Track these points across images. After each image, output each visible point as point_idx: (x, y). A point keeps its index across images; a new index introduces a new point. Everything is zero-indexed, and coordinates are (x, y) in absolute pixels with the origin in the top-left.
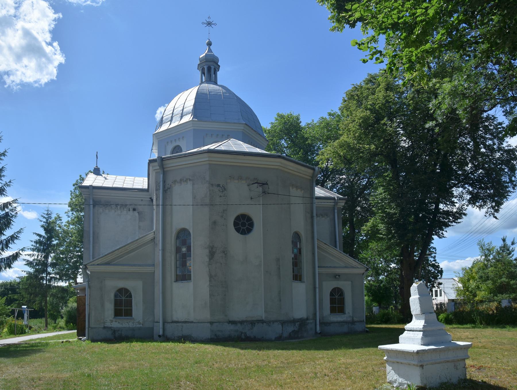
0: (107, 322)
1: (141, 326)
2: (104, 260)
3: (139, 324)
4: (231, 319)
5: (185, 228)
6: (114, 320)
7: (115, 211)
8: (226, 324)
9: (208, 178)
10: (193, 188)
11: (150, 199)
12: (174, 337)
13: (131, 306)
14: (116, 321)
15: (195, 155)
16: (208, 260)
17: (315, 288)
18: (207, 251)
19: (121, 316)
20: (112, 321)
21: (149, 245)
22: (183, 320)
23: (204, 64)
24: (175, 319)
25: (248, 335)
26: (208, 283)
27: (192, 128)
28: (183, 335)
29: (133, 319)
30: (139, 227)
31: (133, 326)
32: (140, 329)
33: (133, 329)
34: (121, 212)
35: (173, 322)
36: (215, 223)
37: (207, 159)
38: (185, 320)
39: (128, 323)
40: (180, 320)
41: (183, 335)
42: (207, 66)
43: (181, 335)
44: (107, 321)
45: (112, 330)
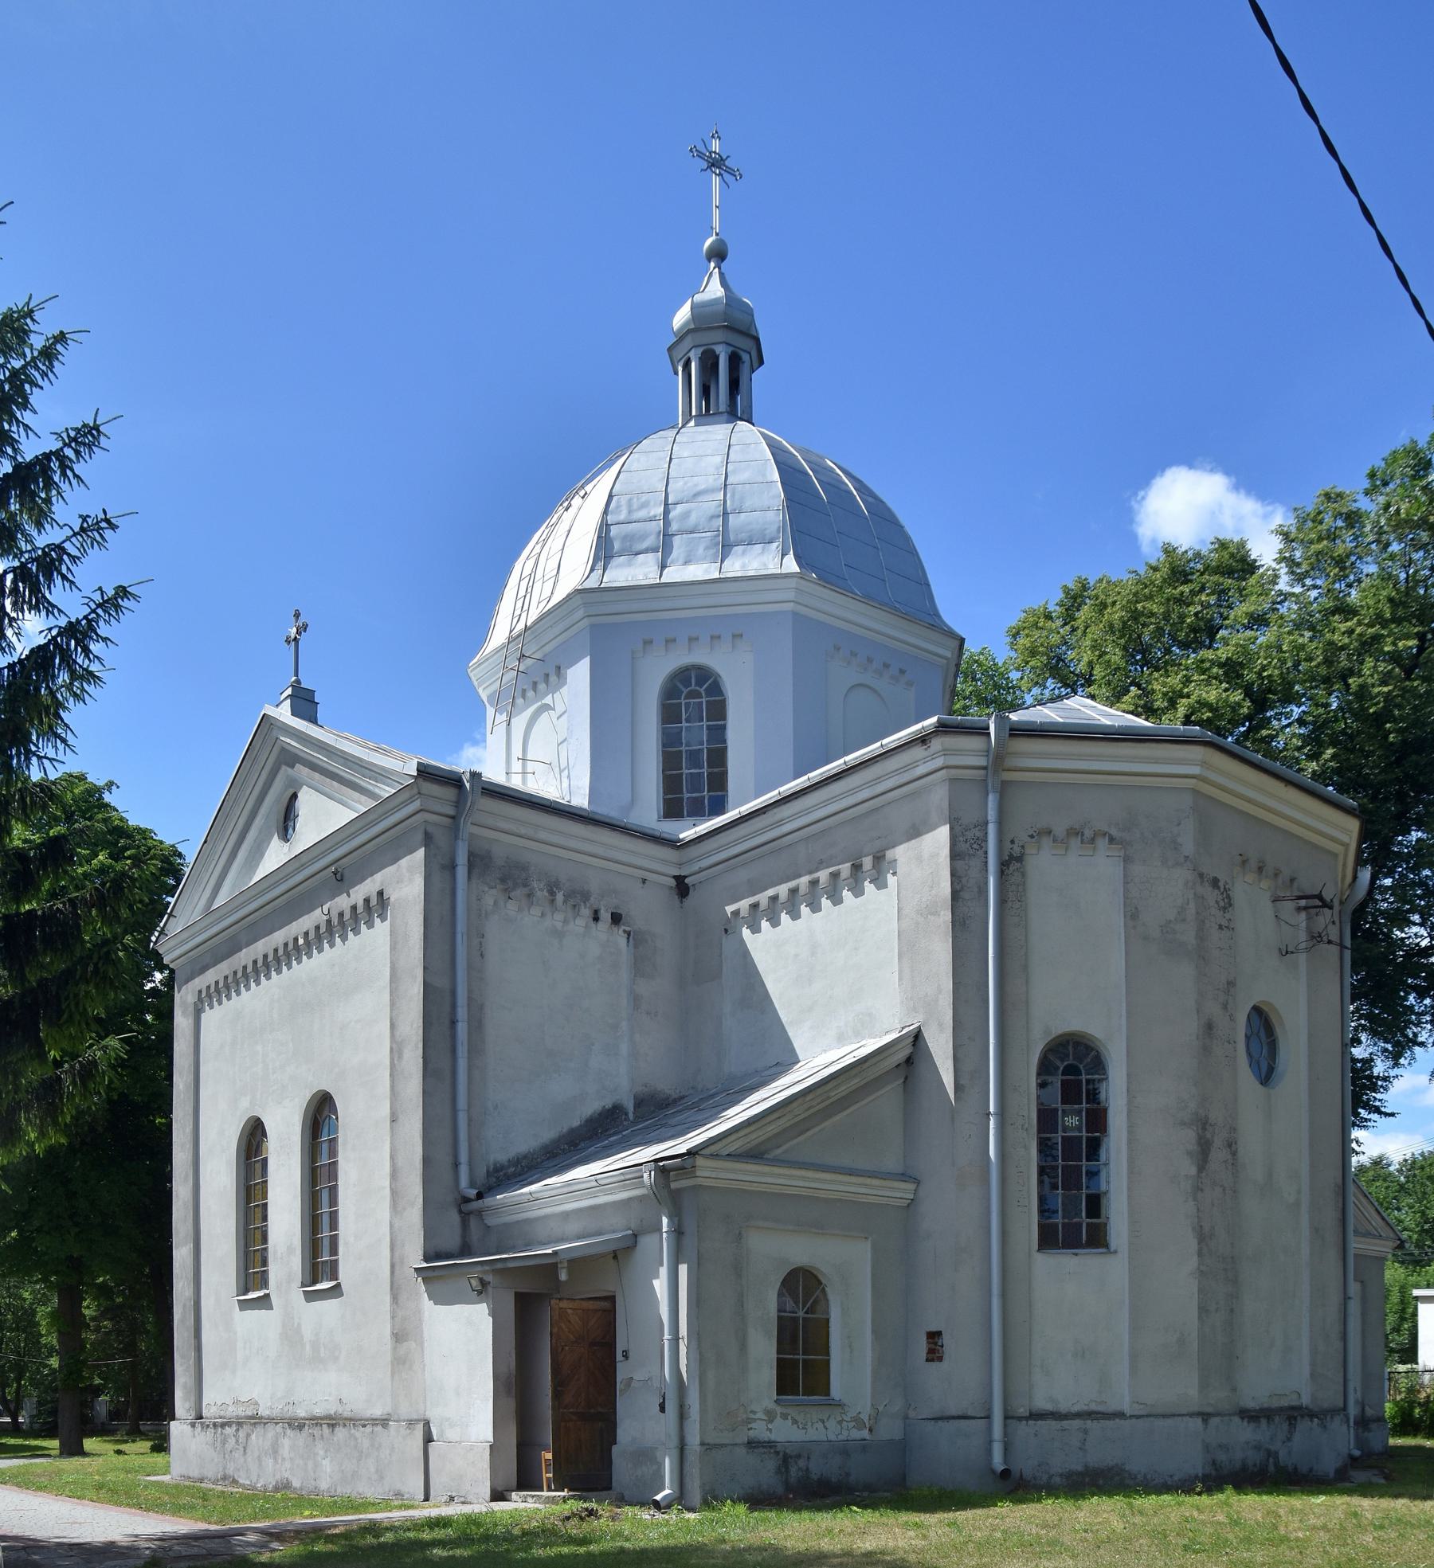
0: (755, 1420)
1: (865, 1434)
2: (753, 1136)
3: (859, 1429)
4: (1251, 1404)
5: (1072, 1034)
6: (779, 1410)
7: (543, 915)
8: (1236, 1419)
9: (1188, 847)
10: (1125, 876)
11: (673, 882)
12: (1051, 1477)
13: (828, 1354)
14: (785, 1416)
15: (1154, 745)
16: (1193, 1171)
17: (1004, 1295)
18: (1190, 1135)
19: (792, 1394)
20: (770, 1416)
21: (888, 1088)
22: (1076, 1409)
23: (719, 336)
24: (1042, 1403)
25: (1282, 1464)
26: (1194, 1261)
27: (790, 606)
28: (1086, 1466)
29: (839, 1405)
30: (636, 1000)
31: (841, 1438)
32: (864, 1446)
33: (844, 1450)
34: (565, 922)
35: (1036, 1416)
36: (1209, 1027)
37: (1195, 770)
38: (1086, 1408)
39: (823, 1422)
40: (1064, 1407)
41: (1086, 1466)
42: (700, 350)
43: (1080, 1468)
44: (754, 1412)
45: (777, 1453)
